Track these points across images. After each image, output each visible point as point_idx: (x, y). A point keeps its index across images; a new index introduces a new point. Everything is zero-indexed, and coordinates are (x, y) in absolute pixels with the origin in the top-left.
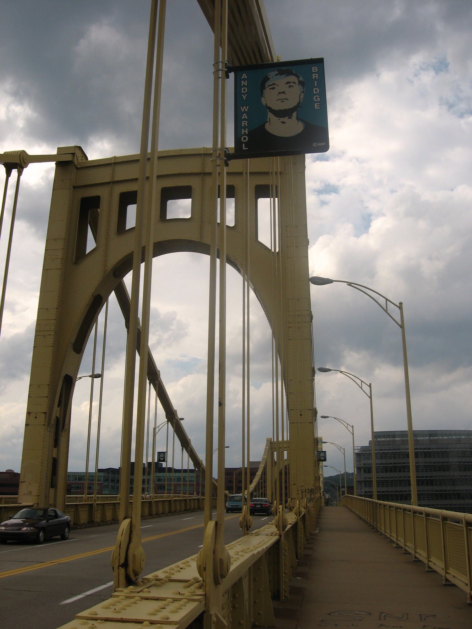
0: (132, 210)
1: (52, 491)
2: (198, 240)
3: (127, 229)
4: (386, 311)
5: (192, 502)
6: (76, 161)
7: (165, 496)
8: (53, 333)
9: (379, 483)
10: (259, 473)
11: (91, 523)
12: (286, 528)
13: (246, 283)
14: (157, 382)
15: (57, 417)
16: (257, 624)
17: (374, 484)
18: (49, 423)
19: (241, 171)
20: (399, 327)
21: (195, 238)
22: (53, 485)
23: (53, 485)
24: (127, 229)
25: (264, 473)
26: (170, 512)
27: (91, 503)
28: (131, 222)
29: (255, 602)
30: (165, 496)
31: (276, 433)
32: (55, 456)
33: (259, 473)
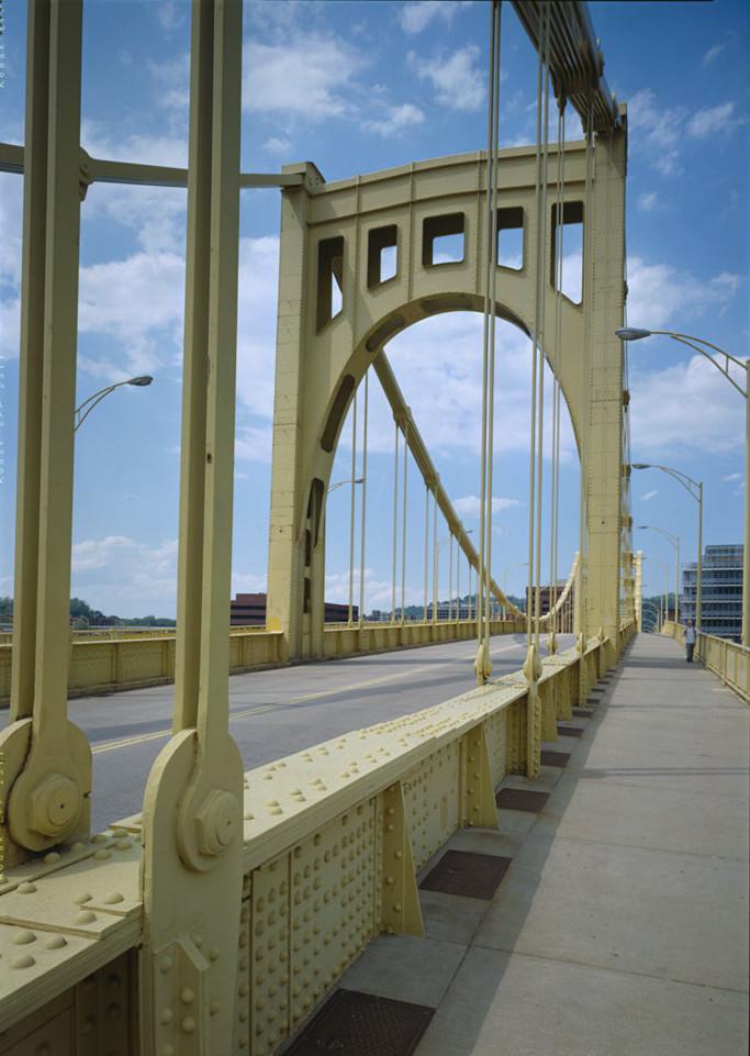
0: (389, 257)
1: (306, 617)
2: (474, 293)
3: (382, 280)
4: (726, 374)
5: (464, 627)
6: (307, 185)
7: (450, 621)
8: (295, 426)
9: (704, 606)
10: (564, 594)
11: (358, 651)
12: (539, 677)
13: (538, 352)
14: (436, 488)
15: (308, 531)
16: (471, 823)
17: (698, 607)
18: (297, 538)
19: (531, 183)
20: (743, 397)
21: (469, 289)
22: (307, 609)
23: (307, 609)
24: (382, 280)
25: (571, 593)
26: (455, 637)
27: (357, 628)
28: (387, 270)
29: (469, 792)
30: (450, 621)
31: (49, 376)
32: (307, 576)
33: (564, 594)
